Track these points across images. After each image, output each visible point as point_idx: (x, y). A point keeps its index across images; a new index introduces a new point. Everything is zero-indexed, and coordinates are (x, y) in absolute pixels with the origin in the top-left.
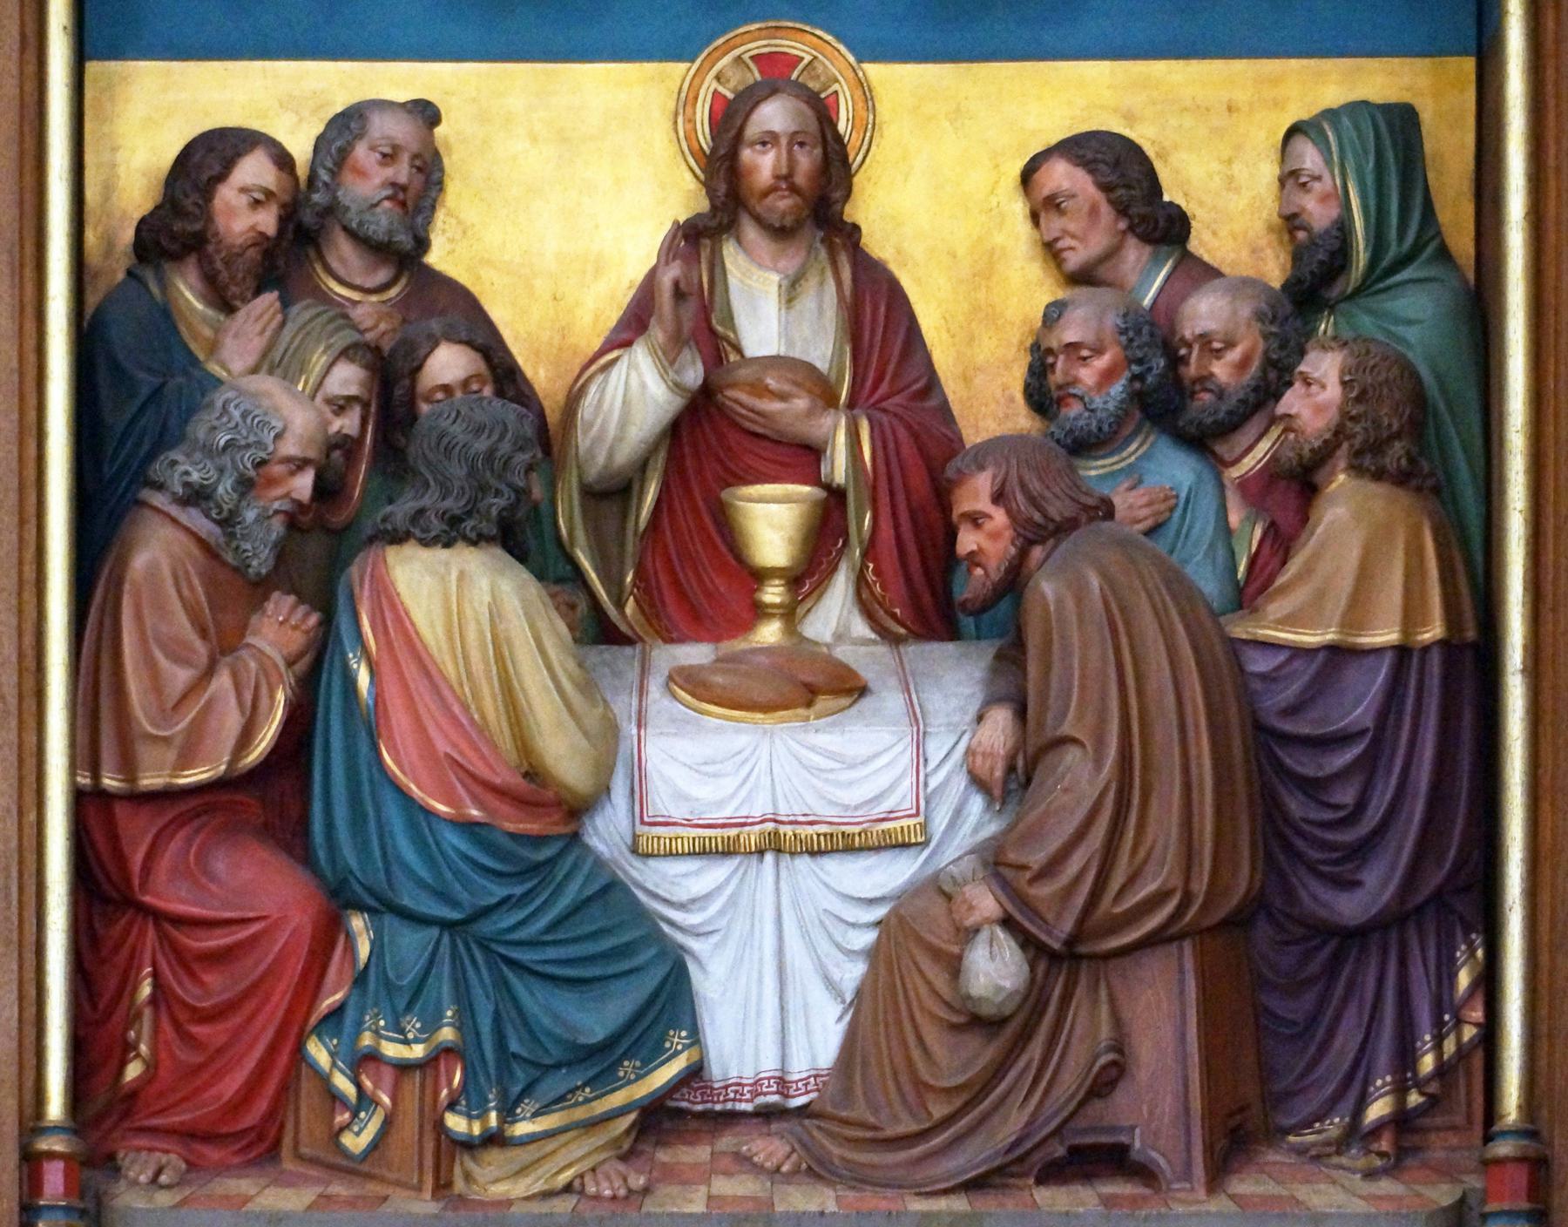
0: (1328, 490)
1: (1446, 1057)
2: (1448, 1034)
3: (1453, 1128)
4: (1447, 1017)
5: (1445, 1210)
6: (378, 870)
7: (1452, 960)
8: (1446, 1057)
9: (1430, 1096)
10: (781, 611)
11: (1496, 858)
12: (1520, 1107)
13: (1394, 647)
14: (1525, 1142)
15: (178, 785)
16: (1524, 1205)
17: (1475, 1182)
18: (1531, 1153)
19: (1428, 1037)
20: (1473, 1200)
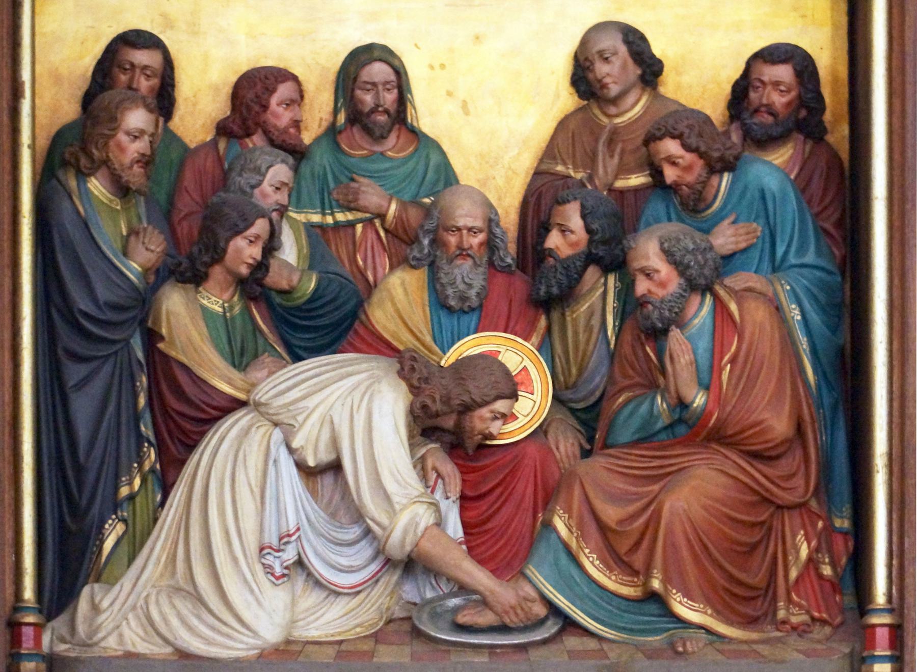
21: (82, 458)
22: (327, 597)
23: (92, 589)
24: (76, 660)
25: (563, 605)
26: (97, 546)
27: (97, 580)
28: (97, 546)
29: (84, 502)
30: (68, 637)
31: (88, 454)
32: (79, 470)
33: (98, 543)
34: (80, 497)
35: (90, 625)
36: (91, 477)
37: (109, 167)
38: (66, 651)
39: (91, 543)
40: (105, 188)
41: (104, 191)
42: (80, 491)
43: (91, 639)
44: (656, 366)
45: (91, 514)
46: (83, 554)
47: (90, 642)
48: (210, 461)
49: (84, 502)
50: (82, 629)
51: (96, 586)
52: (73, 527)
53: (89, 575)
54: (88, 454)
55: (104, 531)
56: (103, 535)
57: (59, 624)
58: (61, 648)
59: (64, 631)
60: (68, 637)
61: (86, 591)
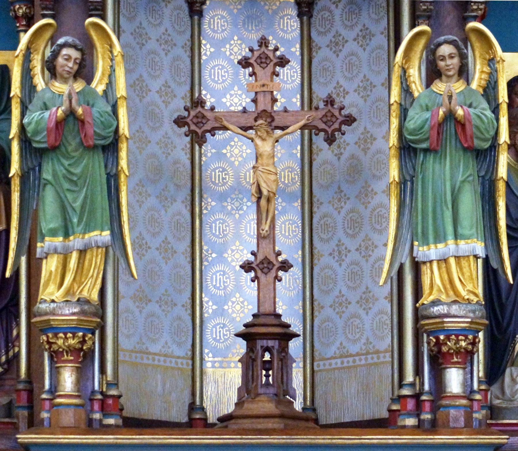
0: (470, 158)
1: (10, 357)
2: (10, 350)
3: (12, 379)
4: (10, 345)
5: (4, 405)
6: (265, 376)
7: (11, 327)
8: (10, 357)
9: (5, 369)
10: (197, 147)
11: (430, 361)
12: (25, 374)
13: (4, 230)
14: (27, 385)
15: (89, 31)
16: (26, 405)
17: (14, 396)
18: (28, 388)
19: (3, 351)
20: (14, 402)
21: (504, 300)
22: (363, 416)
23: (511, 370)
24: (505, 408)
25: (112, 441)
26: (512, 347)
27: (512, 365)
28: (512, 347)
29: (505, 324)
30: (501, 396)
31: (507, 299)
32: (502, 306)
33: (512, 345)
34: (503, 321)
35: (512, 390)
36: (509, 308)
37: (515, 147)
38: (499, 404)
39: (509, 345)
40: (512, 158)
41: (512, 160)
42: (503, 318)
43: (513, 397)
44: (513, 358)
45: (510, 330)
46: (505, 351)
47: (512, 399)
48: (333, 430)
49: (505, 324)
50: (508, 391)
51: (513, 368)
52: (499, 337)
53: (507, 362)
54: (507, 299)
55: (516, 339)
56: (515, 341)
57: (495, 389)
58: (496, 402)
59: (498, 393)
60: (501, 396)
61: (508, 371)
